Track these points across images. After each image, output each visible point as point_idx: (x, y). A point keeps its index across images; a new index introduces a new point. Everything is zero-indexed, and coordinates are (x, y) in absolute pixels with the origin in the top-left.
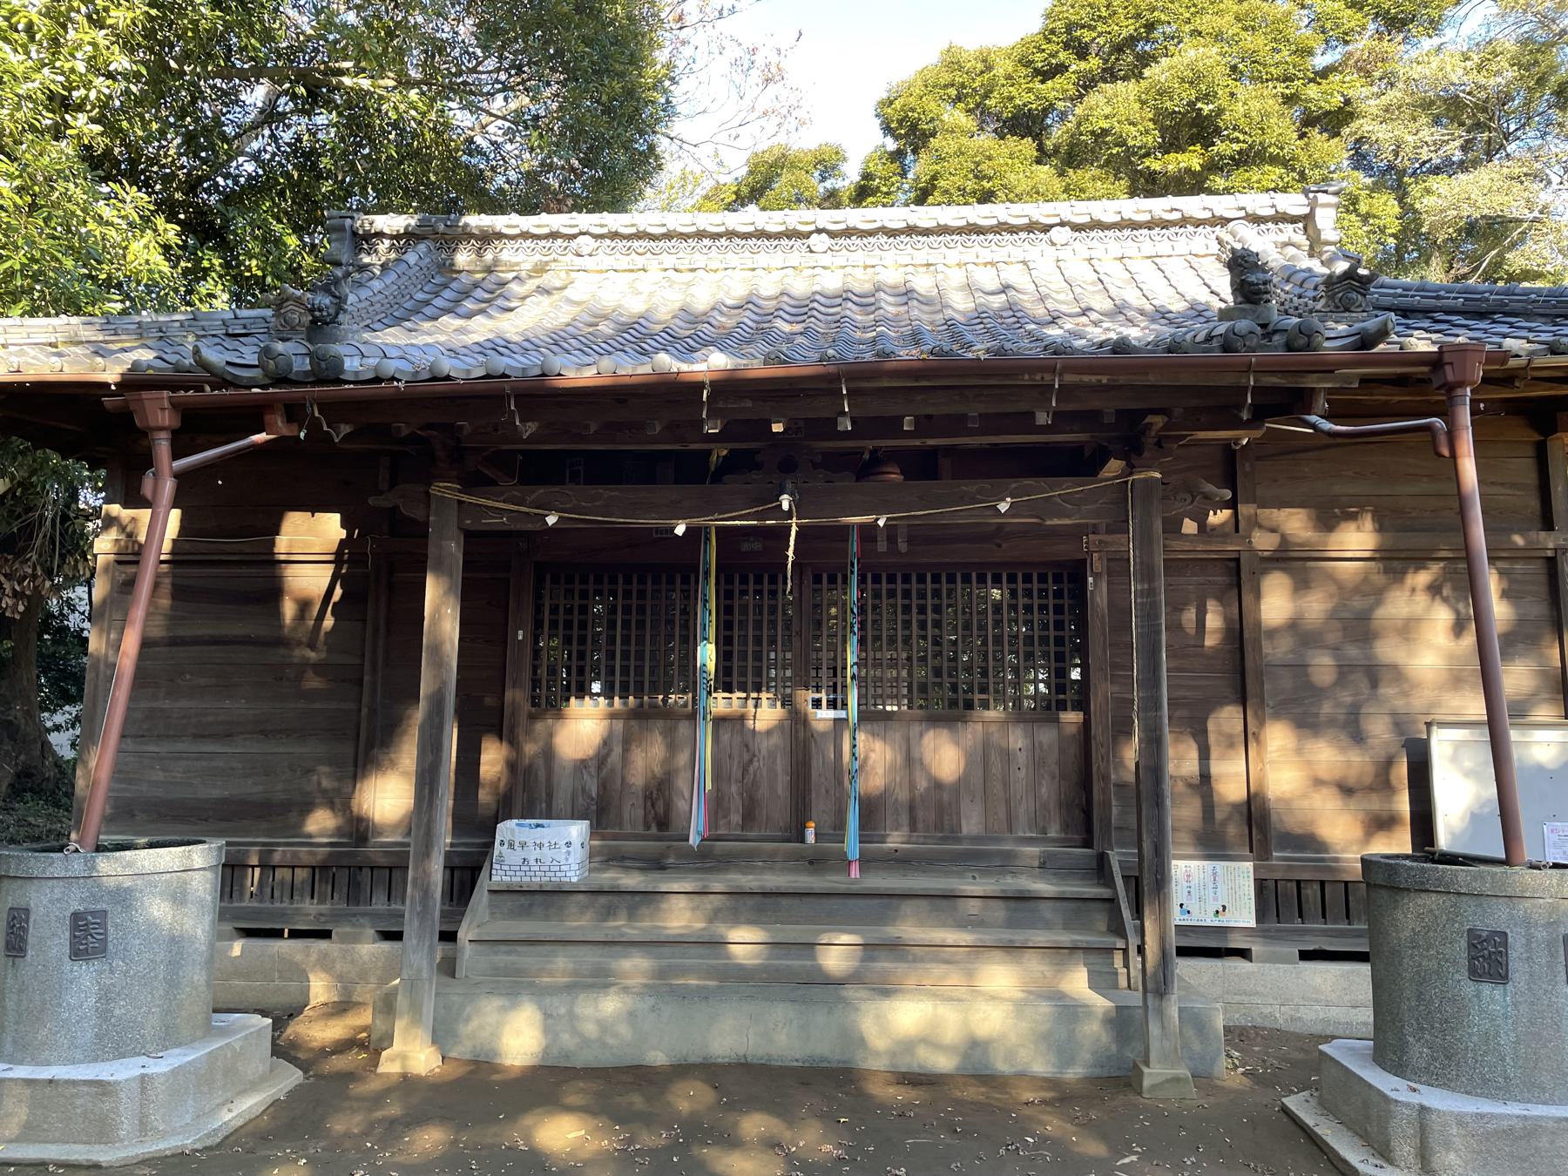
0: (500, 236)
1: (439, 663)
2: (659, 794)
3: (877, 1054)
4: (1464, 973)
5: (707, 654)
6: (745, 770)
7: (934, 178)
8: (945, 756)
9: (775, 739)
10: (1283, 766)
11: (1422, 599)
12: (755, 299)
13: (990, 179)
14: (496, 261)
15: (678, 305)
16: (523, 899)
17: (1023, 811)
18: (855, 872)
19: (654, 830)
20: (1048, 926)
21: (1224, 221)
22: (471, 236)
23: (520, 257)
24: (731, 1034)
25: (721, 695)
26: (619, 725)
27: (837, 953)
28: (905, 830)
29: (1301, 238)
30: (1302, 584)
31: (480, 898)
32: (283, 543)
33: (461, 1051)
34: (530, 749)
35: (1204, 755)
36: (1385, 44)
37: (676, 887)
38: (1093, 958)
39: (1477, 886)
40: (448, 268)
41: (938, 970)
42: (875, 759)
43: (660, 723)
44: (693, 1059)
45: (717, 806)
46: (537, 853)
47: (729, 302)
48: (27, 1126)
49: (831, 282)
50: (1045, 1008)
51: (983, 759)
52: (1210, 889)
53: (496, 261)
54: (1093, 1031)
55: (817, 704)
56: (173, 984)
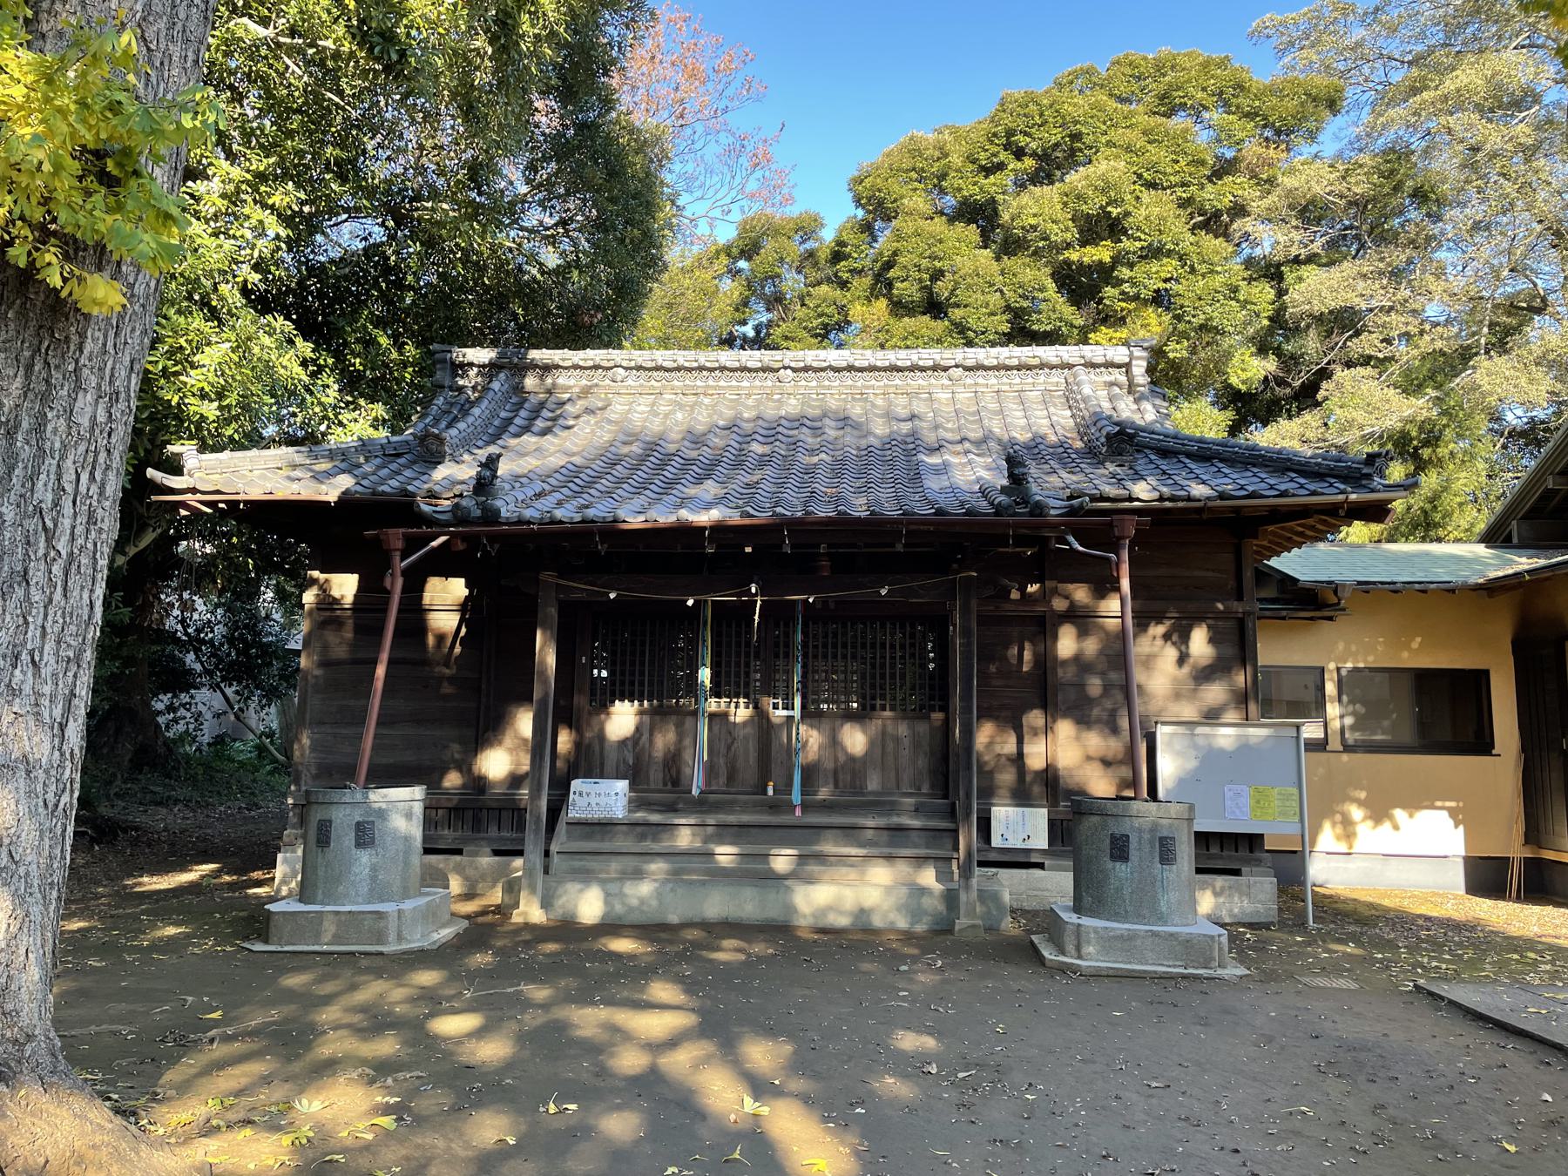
0: (557, 367)
1: (545, 682)
2: (673, 761)
3: (805, 916)
4: (1107, 859)
5: (705, 675)
6: (729, 748)
7: (895, 254)
8: (855, 740)
9: (749, 730)
10: (1065, 748)
11: (1159, 642)
12: (738, 422)
13: (941, 259)
14: (554, 385)
15: (684, 427)
16: (587, 829)
17: (906, 777)
18: (798, 812)
19: (669, 786)
20: (916, 846)
21: (1070, 366)
22: (536, 366)
23: (572, 382)
24: (716, 905)
25: (714, 700)
26: (646, 718)
27: (782, 860)
28: (831, 786)
29: (1123, 379)
30: (1083, 633)
31: (561, 827)
32: (427, 598)
33: (558, 912)
34: (588, 735)
35: (1020, 742)
36: (1271, 151)
37: (683, 821)
38: (940, 864)
39: (1115, 811)
40: (518, 389)
41: (844, 870)
42: (812, 739)
43: (674, 718)
44: (697, 920)
45: (711, 770)
46: (597, 800)
47: (721, 423)
48: (334, 936)
49: (792, 407)
50: (904, 890)
51: (879, 744)
52: (1019, 825)
53: (554, 385)
54: (933, 904)
55: (775, 707)
56: (407, 863)
